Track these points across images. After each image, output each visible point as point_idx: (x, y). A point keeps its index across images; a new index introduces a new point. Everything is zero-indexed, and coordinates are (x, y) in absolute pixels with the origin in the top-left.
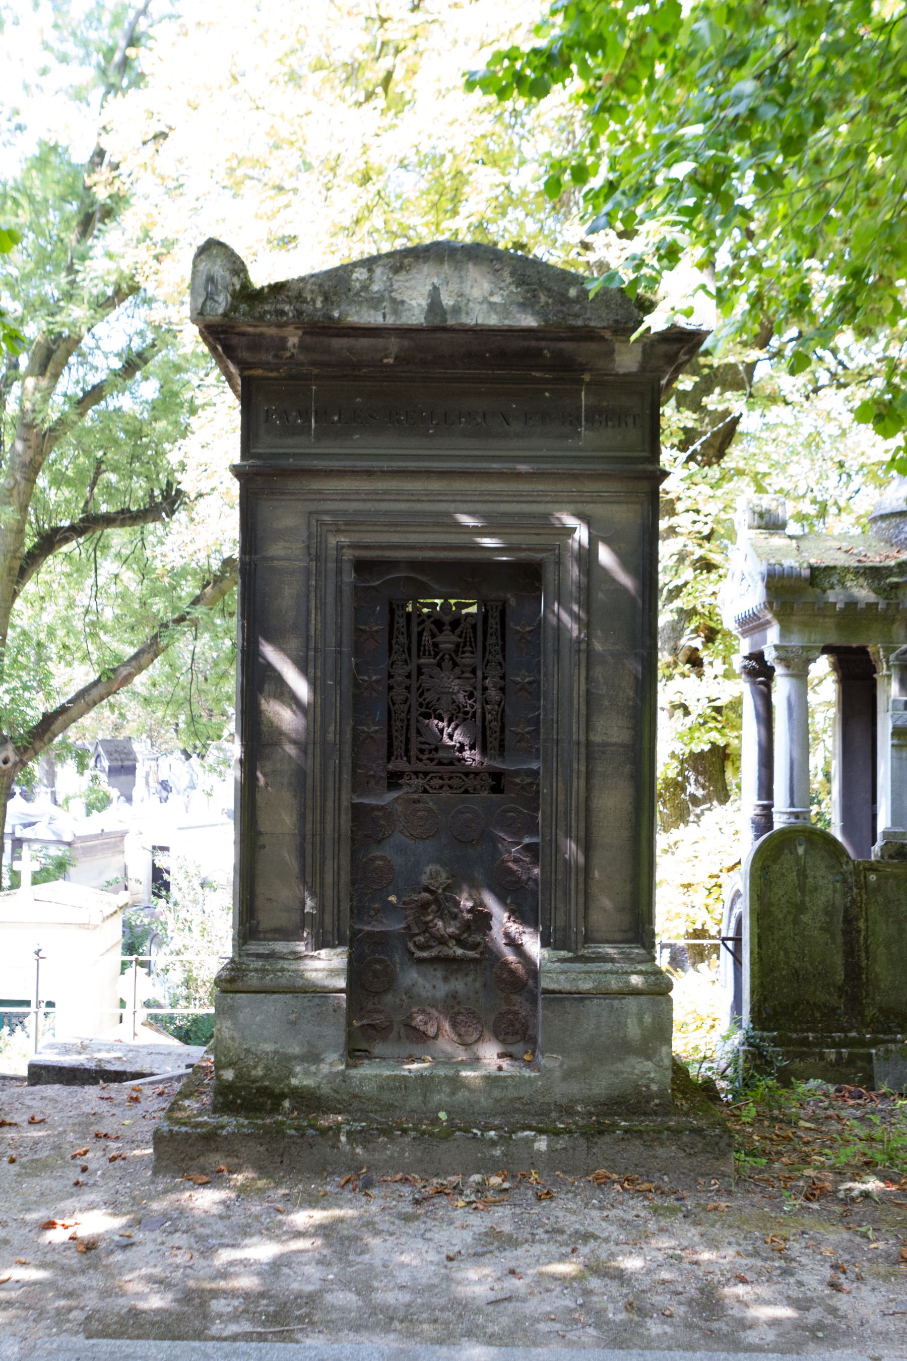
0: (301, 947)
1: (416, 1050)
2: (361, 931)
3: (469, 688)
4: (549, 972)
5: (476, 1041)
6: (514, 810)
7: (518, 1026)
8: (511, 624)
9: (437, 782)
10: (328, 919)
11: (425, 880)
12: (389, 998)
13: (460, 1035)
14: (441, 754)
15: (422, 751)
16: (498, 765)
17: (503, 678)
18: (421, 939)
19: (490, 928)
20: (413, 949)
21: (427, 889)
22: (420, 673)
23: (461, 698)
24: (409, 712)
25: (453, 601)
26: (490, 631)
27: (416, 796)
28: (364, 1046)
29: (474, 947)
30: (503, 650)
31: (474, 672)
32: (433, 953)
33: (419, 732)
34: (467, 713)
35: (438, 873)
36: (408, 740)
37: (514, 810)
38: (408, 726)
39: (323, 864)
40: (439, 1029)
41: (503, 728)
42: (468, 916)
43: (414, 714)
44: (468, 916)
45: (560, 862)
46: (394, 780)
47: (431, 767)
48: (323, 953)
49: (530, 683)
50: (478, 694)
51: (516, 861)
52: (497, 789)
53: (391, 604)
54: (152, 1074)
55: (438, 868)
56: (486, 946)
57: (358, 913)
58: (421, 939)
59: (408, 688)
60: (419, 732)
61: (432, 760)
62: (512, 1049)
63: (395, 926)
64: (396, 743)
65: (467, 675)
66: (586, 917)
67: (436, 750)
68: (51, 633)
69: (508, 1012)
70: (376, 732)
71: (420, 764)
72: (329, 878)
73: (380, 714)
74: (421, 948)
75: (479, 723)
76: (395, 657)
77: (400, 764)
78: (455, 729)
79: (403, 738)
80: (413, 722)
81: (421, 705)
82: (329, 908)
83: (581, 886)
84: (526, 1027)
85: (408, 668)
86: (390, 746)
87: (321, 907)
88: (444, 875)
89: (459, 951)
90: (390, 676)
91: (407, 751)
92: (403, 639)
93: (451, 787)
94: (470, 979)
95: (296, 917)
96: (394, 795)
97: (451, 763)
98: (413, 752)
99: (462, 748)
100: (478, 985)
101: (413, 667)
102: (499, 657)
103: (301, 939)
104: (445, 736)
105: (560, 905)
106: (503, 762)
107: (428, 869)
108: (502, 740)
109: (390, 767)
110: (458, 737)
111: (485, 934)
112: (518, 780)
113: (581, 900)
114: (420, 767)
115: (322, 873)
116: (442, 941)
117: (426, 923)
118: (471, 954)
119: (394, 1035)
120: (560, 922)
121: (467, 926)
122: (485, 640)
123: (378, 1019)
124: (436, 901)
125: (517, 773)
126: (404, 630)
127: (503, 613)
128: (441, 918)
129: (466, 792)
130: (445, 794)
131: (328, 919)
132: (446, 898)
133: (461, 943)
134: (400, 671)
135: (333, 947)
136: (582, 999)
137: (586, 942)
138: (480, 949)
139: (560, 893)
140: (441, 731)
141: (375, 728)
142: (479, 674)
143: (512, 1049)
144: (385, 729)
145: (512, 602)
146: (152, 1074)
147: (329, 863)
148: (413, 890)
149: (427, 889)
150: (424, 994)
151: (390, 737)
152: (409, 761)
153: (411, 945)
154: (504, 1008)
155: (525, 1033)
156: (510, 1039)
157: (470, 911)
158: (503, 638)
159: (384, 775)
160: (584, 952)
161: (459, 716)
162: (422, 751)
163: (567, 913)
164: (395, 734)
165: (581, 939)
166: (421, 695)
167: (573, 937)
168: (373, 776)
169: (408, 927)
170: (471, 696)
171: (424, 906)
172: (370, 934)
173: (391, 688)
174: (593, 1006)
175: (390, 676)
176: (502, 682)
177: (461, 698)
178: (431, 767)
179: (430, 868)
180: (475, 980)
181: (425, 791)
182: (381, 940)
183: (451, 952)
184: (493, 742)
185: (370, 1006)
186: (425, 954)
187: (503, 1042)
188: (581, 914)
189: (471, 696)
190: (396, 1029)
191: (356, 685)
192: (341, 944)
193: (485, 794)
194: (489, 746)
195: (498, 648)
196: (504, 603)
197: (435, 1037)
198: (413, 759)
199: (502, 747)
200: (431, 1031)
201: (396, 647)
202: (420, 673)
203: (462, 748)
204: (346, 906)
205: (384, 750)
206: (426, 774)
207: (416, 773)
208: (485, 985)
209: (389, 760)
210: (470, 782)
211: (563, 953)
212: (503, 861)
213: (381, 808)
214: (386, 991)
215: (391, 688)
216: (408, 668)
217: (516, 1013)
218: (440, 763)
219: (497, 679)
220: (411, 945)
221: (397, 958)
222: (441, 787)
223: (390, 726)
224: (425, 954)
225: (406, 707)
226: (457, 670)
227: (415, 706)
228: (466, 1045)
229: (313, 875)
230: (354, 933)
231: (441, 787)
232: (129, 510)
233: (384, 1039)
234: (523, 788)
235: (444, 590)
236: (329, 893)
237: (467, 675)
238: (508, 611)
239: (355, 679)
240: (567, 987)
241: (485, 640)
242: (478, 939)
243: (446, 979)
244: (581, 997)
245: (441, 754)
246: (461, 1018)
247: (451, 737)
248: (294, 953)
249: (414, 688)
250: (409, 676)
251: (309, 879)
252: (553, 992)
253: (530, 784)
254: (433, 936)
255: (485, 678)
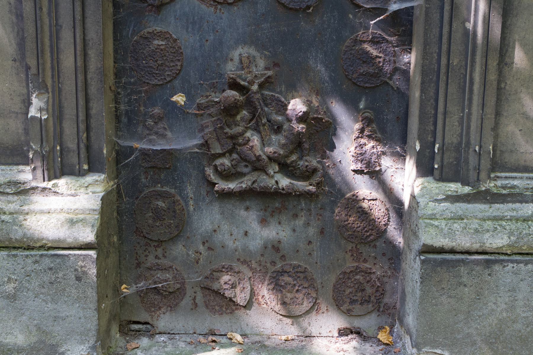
0: (26, 175)
1: (220, 323)
2: (132, 150)
4: (433, 217)
5: (308, 312)
7: (369, 291)
10: (69, 129)
11: (231, 69)
12: (178, 249)
13: (284, 303)
18: (226, 162)
19: (333, 147)
20: (213, 177)
21: (234, 85)
28: (144, 316)
29: (307, 175)
32: (244, 183)
35: (251, 60)
39: (56, 37)
40: (253, 293)
42: (300, 127)
44: (300, 127)
45: (457, 36)
48: (62, 183)
51: (375, 41)
55: (252, 51)
56: (326, 175)
57: (126, 120)
58: (226, 162)
62: (358, 323)
63: (185, 142)
66: (496, 128)
68: (121, 43)
69: (357, 271)
72: (68, 61)
74: (226, 176)
82: (69, 111)
83: (492, 77)
84: (381, 292)
87: (57, 110)
88: (262, 63)
89: (284, 182)
94: (300, 222)
95: (15, 126)
100: (312, 231)
103: (26, 162)
105: (453, 108)
107: (236, 54)
111: (324, 156)
113: (491, 101)
115: (56, 50)
116: (258, 166)
117: (233, 137)
118: (302, 185)
119: (186, 301)
120: (452, 138)
121: (297, 144)
123: (165, 279)
124: (249, 104)
128: (256, 129)
131: (69, 129)
132: (264, 99)
133: (286, 168)
135: (81, 174)
136: (488, 263)
137: (493, 169)
138: (317, 178)
139: (453, 89)
143: (358, 323)
147: (66, 36)
148: (213, 87)
149: (234, 85)
150: (230, 244)
153: (209, 171)
154: (350, 264)
155: (379, 301)
156: (357, 309)
157: (303, 119)
160: (491, 185)
163: (464, 122)
165: (485, 164)
167: (473, 160)
169: (206, 145)
171: (230, 111)
172: (144, 153)
174: (506, 274)
179: (239, 52)
180: (307, 224)
182: (164, 163)
183: (271, 183)
185: (151, 260)
186: (232, 186)
187: (348, 313)
188: (489, 124)
190: (189, 292)
192: (92, 170)
197: (248, 306)
200: (241, 298)
204: (102, 108)
208: (322, 232)
211: (454, 187)
212: (357, 42)
214: (173, 239)
217: (368, 273)
220: (209, 171)
221: (190, 191)
224: (232, 186)
228: (293, 317)
229: (39, 55)
230: (121, 155)
233: (173, 307)
236: (69, 86)
240: (465, 242)
242: (314, 163)
243: (263, 222)
244: (491, 258)
246: (286, 279)
248: (16, 183)
251: (32, 62)
252: (441, 251)
254: (244, 159)
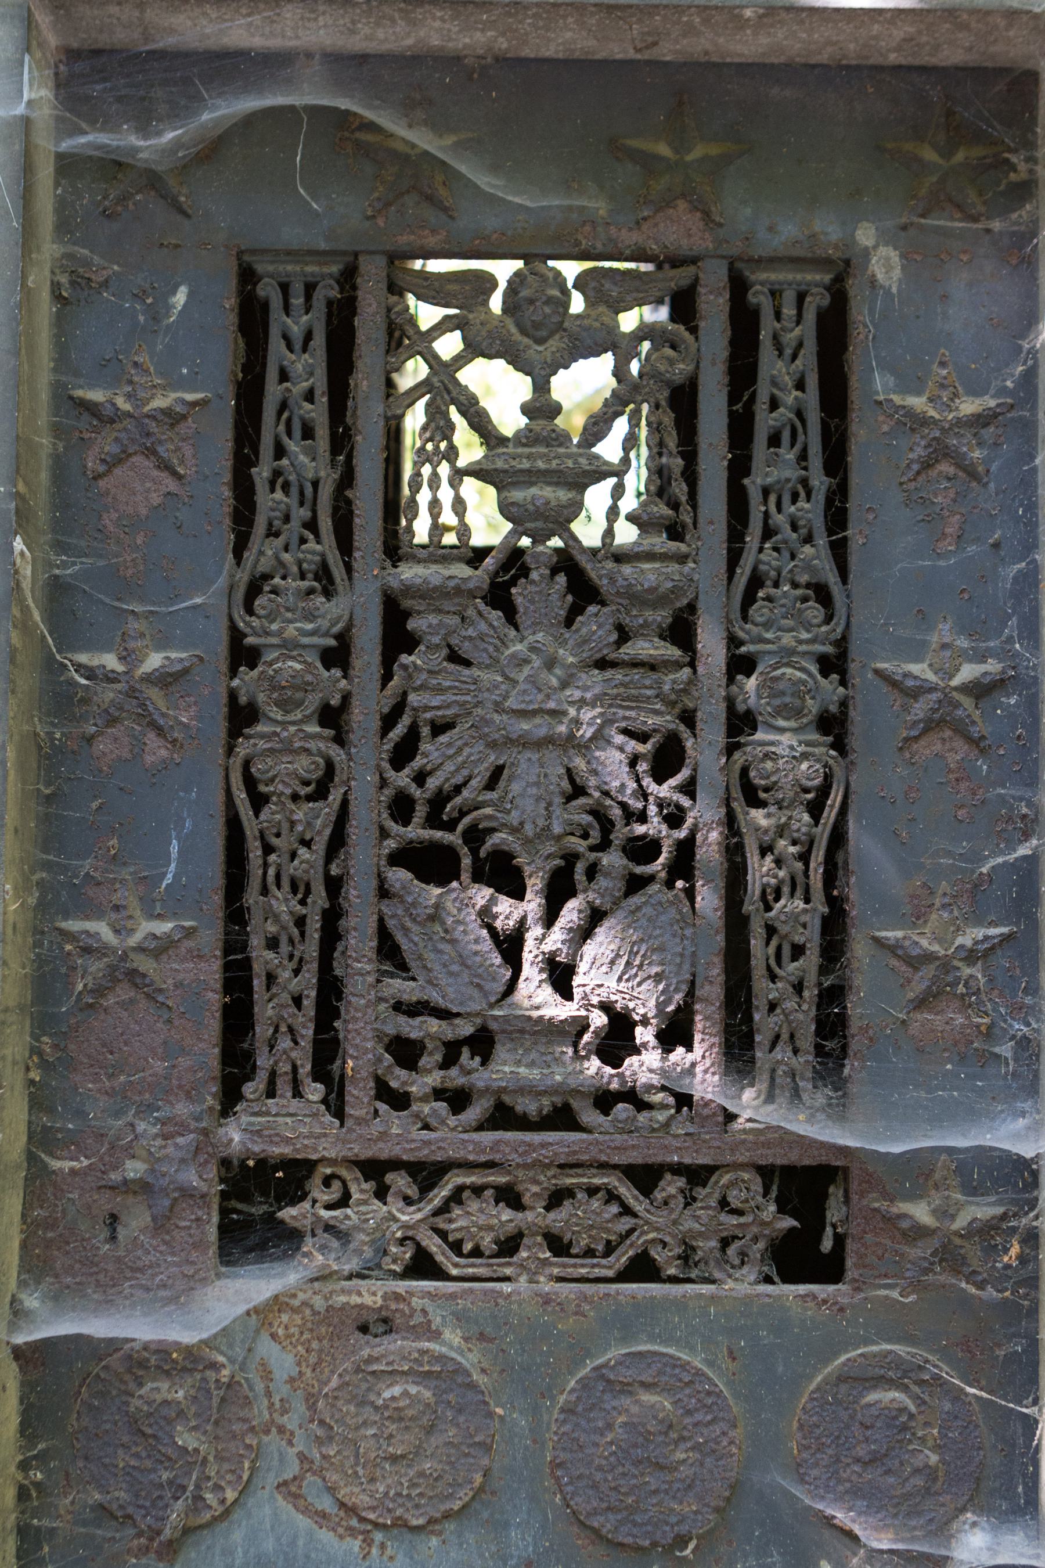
3: (659, 720)
6: (899, 1374)
8: (875, 382)
9: (483, 1219)
14: (508, 1069)
15: (406, 1052)
16: (814, 1126)
17: (835, 664)
22: (397, 639)
23: (614, 768)
24: (338, 841)
25: (570, 269)
26: (765, 422)
27: (370, 1295)
30: (837, 517)
31: (681, 632)
33: (390, 952)
34: (644, 850)
36: (330, 992)
37: (899, 1374)
38: (332, 917)
41: (835, 924)
43: (364, 856)
46: (256, 1209)
47: (453, 1136)
49: (981, 690)
50: (704, 750)
52: (804, 1257)
53: (247, 276)
54: (349, 569)
59: (333, 717)
60: (390, 952)
61: (458, 1100)
64: (266, 1011)
65: (646, 648)
67: (482, 1043)
70: (160, 948)
71: (396, 1123)
73: (186, 853)
75: (708, 899)
76: (263, 552)
77: (285, 1123)
78: (584, 933)
79: (308, 982)
80: (358, 895)
81: (401, 808)
85: (331, 612)
86: (237, 1019)
90: (242, 654)
91: (326, 1051)
92: (310, 461)
93: (558, 1246)
96: (254, 1286)
97: (562, 1118)
98: (361, 1057)
99: (618, 1038)
101: (358, 605)
102: (816, 556)
104: (531, 973)
106: (839, 1110)
108: (833, 996)
109: (234, 1136)
110: (598, 974)
112: (921, 1212)
114: (397, 1135)
122: (739, 467)
125: (917, 1172)
126: (318, 412)
127: (834, 331)
129: (642, 1269)
130: (529, 1285)
134: (291, 627)
140: (510, 945)
141: (157, 924)
142: (711, 643)
144: (211, 937)
145: (886, 266)
146: (349, 569)
151: (237, 978)
152: (336, 1105)
158: (836, 459)
159: (202, 1179)
161: (603, 862)
162: (406, 1052)
164: (262, 958)
166: (403, 753)
168: (143, 1188)
170: (667, 759)
173: (241, 716)
175: (242, 654)
176: (830, 689)
177: (614, 768)
178: (453, 1136)
181: (423, 1266)
184: (785, 1005)
189: (667, 759)
191: (61, 699)
193: (743, 1285)
194: (765, 1024)
195: (811, 511)
196: (841, 274)
198: (359, 1096)
199: (832, 1028)
201: (269, 502)
202: (397, 639)
203: (618, 1038)
205: (206, 1048)
206: (427, 1174)
207: (375, 1170)
209: (230, 1097)
210: (662, 1221)
213: (189, 1362)
215: (241, 716)
216: (331, 612)
218: (503, 1117)
219: (801, 672)
222: (509, 1246)
223: (236, 915)
225: (326, 810)
226: (596, 625)
227: (368, 811)
231: (509, 1246)
232: (325, 1101)
234: (949, 1256)
235: (529, 200)
237: (646, 648)
238: (862, 317)
239: (52, 668)
241: (739, 467)
245: (508, 1069)
247: (560, 976)
249: (364, 717)
250: (338, 655)
253: (987, 1233)
255: (740, 665)
